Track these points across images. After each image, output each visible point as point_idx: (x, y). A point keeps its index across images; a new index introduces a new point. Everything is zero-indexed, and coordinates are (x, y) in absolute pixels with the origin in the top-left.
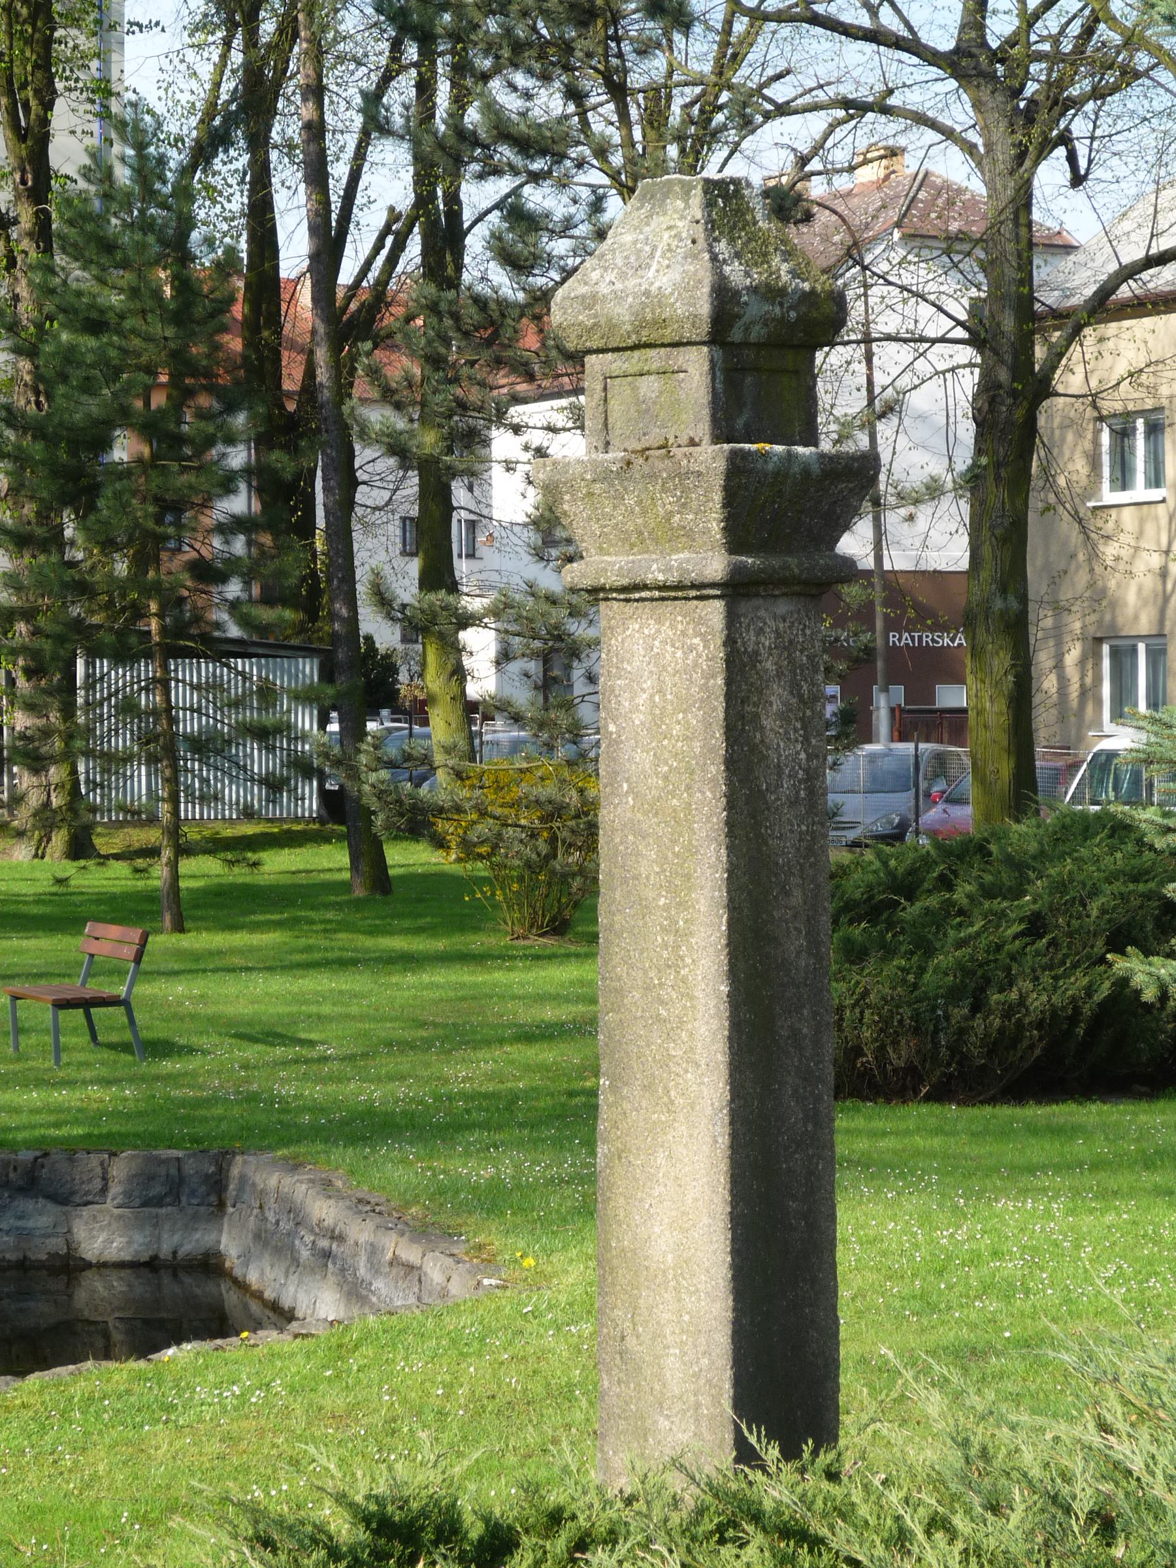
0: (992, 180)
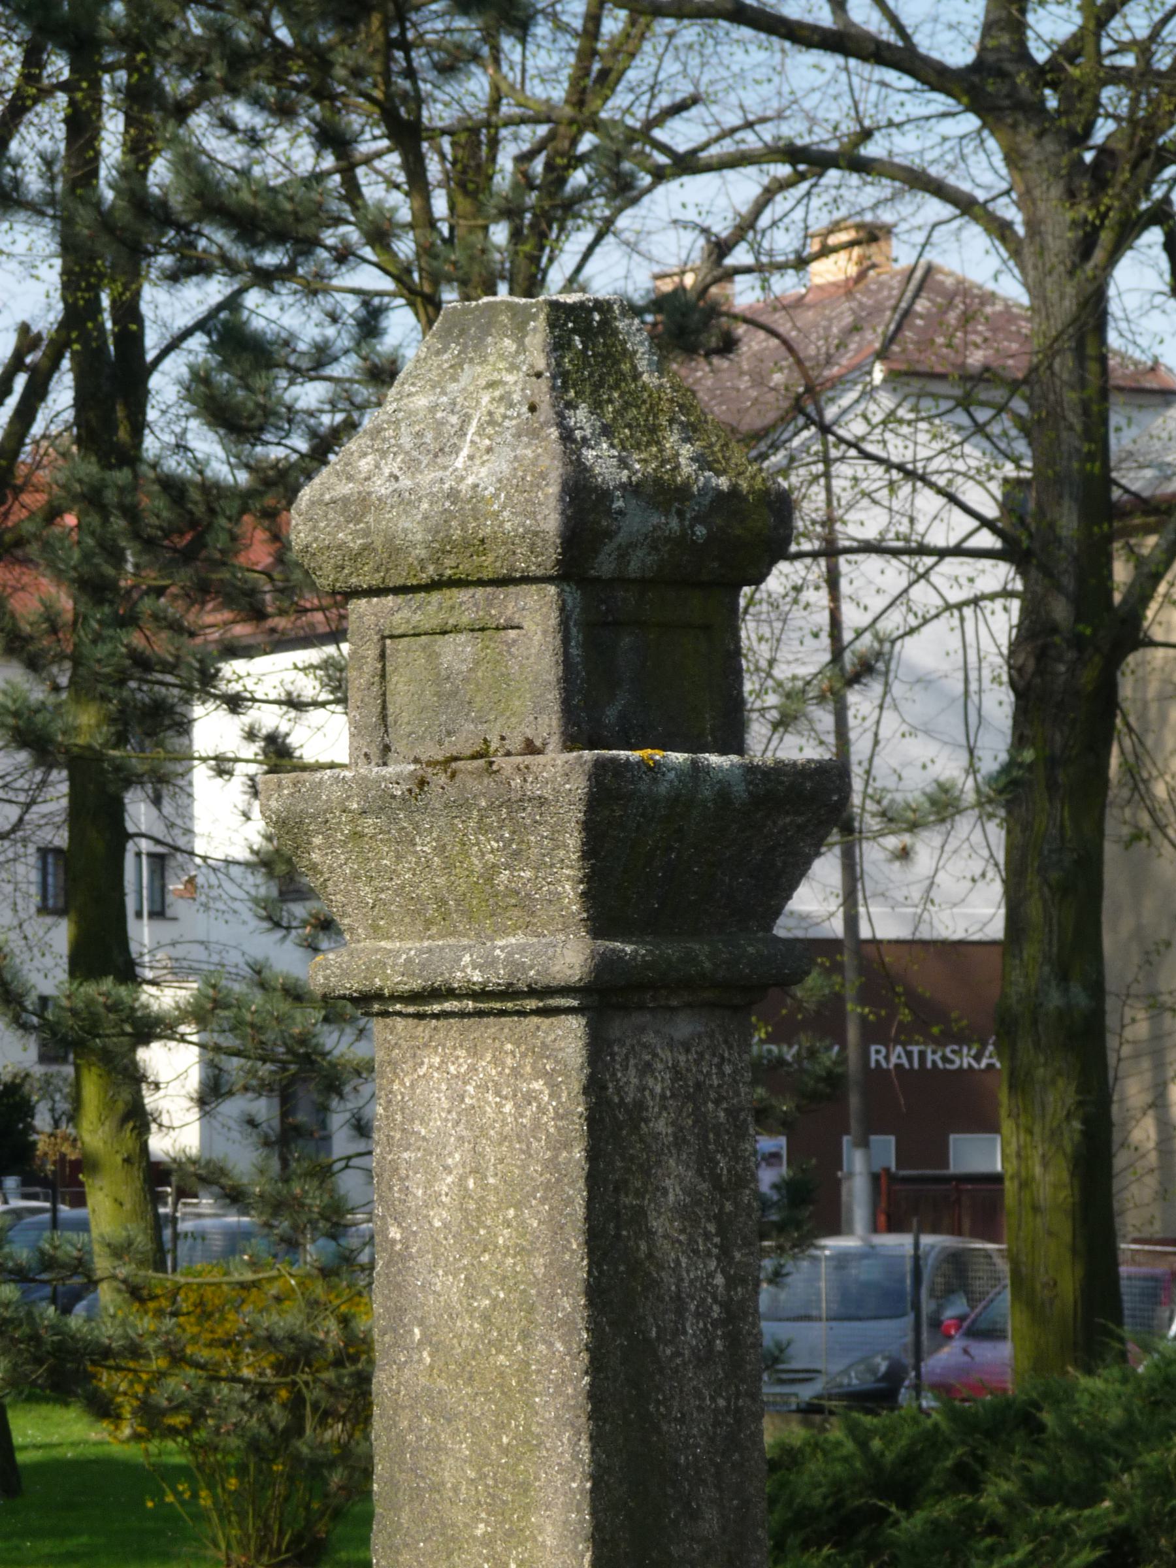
0: (1041, 283)
